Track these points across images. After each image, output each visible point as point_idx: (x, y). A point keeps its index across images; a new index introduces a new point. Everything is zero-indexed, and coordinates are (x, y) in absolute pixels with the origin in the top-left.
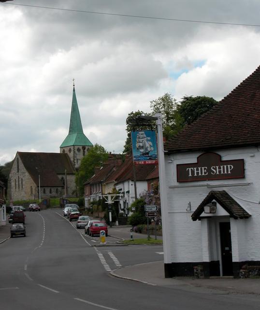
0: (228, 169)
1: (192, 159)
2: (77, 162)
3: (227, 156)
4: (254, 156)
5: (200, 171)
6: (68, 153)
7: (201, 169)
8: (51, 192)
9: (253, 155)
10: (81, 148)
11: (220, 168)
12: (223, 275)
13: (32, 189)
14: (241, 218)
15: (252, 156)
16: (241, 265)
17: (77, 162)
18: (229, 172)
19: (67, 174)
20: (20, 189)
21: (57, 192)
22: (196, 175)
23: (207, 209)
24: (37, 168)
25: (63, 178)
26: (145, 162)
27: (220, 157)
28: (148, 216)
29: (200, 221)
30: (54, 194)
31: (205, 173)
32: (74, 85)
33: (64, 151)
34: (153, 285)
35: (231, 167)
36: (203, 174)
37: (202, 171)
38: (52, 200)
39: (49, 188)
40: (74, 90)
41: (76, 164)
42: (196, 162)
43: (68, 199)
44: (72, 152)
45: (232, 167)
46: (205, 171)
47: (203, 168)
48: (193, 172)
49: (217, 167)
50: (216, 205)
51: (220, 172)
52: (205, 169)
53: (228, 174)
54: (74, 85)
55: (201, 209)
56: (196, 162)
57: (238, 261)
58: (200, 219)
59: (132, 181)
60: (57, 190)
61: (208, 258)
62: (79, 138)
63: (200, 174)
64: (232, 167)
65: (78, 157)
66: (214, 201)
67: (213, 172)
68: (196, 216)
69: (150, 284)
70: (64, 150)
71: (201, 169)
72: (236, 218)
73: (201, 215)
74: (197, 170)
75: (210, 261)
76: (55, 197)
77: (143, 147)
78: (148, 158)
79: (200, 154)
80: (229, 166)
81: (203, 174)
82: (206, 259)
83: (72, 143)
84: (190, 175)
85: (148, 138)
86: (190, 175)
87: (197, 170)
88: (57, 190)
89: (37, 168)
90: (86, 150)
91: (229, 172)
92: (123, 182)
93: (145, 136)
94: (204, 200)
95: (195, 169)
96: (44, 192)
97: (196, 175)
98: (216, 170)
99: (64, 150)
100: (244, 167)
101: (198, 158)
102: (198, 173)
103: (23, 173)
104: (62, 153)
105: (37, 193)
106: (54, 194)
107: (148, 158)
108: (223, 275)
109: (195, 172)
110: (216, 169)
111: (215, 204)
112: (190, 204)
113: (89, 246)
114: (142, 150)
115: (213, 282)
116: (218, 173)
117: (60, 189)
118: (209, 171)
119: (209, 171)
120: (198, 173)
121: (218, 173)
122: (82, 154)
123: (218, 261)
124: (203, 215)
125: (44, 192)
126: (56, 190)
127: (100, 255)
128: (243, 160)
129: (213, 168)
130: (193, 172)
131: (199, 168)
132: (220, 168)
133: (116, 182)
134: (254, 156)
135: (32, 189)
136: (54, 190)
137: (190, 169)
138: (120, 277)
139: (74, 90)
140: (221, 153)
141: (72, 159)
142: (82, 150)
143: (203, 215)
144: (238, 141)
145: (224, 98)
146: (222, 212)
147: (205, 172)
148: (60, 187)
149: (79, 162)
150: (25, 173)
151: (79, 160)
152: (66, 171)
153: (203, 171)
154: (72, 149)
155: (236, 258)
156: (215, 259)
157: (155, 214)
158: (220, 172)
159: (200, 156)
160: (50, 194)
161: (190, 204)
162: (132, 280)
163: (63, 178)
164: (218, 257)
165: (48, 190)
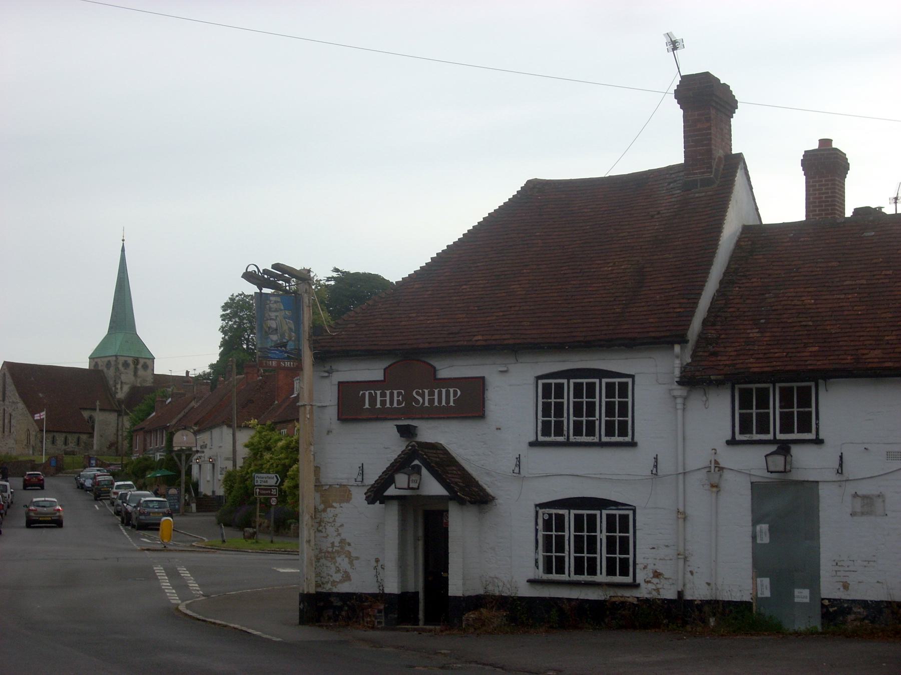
0: (450, 397)
1: (372, 371)
2: (121, 388)
3: (448, 369)
4: (506, 372)
5: (388, 398)
6: (105, 370)
7: (392, 395)
8: (66, 443)
9: (505, 369)
10: (130, 361)
11: (431, 394)
12: (426, 623)
13: (29, 435)
14: (473, 503)
15: (501, 372)
16: (476, 602)
17: (121, 388)
18: (452, 404)
19: (100, 410)
20: (6, 433)
21: (78, 444)
22: (378, 406)
23: (401, 479)
24: (41, 395)
25: (91, 417)
26: (279, 364)
27: (435, 370)
28: (260, 494)
29: (383, 505)
30: (72, 446)
31: (399, 403)
32: (123, 240)
33: (96, 364)
34: (275, 639)
35: (455, 393)
36: (395, 405)
37: (394, 398)
38: (68, 459)
39: (64, 435)
40: (123, 250)
41: (119, 390)
42: (383, 379)
43: (99, 457)
44: (112, 369)
45: (459, 393)
46: (400, 398)
47: (395, 392)
48: (373, 399)
49: (426, 391)
50: (419, 472)
51: (431, 401)
52: (399, 394)
53: (448, 408)
54: (123, 240)
55: (387, 479)
56: (383, 379)
57: (460, 594)
58: (384, 500)
59: (229, 426)
60: (78, 439)
61: (396, 585)
62: (127, 342)
63: (388, 405)
64: (459, 393)
65: (123, 378)
66: (416, 462)
67: (417, 402)
68: (376, 494)
69: (268, 636)
70: (96, 363)
71: (392, 395)
72: (461, 502)
73: (386, 493)
74: (383, 395)
75: (400, 592)
76: (73, 453)
77: (276, 330)
78: (286, 355)
79: (394, 361)
80: (451, 390)
81: (395, 405)
82: (392, 587)
83: (111, 352)
84: (367, 406)
85: (287, 312)
86: (367, 406)
87: (383, 395)
88: (78, 439)
89: (41, 395)
90: (139, 366)
91: (452, 404)
92: (211, 428)
93: (282, 308)
94: (395, 460)
95: (378, 392)
96: (53, 442)
97: (378, 406)
98: (423, 398)
99: (96, 363)
100: (484, 394)
101: (385, 370)
102: (383, 403)
103: (13, 402)
104: (93, 368)
105: (40, 445)
106: (72, 446)
107: (286, 355)
108: (426, 623)
109: (379, 399)
110: (423, 396)
111: (417, 470)
112: (362, 468)
113: (136, 550)
114: (274, 337)
115: (406, 636)
116: (426, 404)
117: (84, 437)
118: (408, 398)
119: (408, 398)
120: (383, 403)
121: (426, 404)
122: (133, 373)
123: (417, 593)
124: (391, 491)
125: (53, 442)
126: (75, 440)
127: (159, 571)
128: (483, 378)
129: (417, 393)
130: (373, 399)
131: (388, 392)
132: (431, 394)
133: (196, 428)
134: (506, 372)
135: (29, 435)
136: (72, 439)
137: (367, 393)
138: (201, 617)
139: (123, 250)
140: (437, 363)
141: (111, 383)
142: (132, 366)
143: (391, 491)
144: (602, 269)
145: (468, 231)
146: (433, 487)
147: (398, 401)
148: (84, 433)
149: (126, 389)
150: (17, 403)
151: (125, 383)
152: (98, 403)
153: (396, 399)
154: (113, 363)
155: (456, 588)
156: (411, 588)
157: (274, 492)
158: (431, 401)
159: (389, 366)
160: (64, 447)
161: (362, 468)
162: (246, 632)
163: (91, 417)
164: (416, 584)
165: (60, 438)
